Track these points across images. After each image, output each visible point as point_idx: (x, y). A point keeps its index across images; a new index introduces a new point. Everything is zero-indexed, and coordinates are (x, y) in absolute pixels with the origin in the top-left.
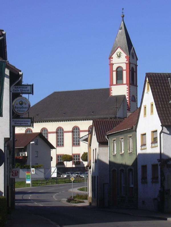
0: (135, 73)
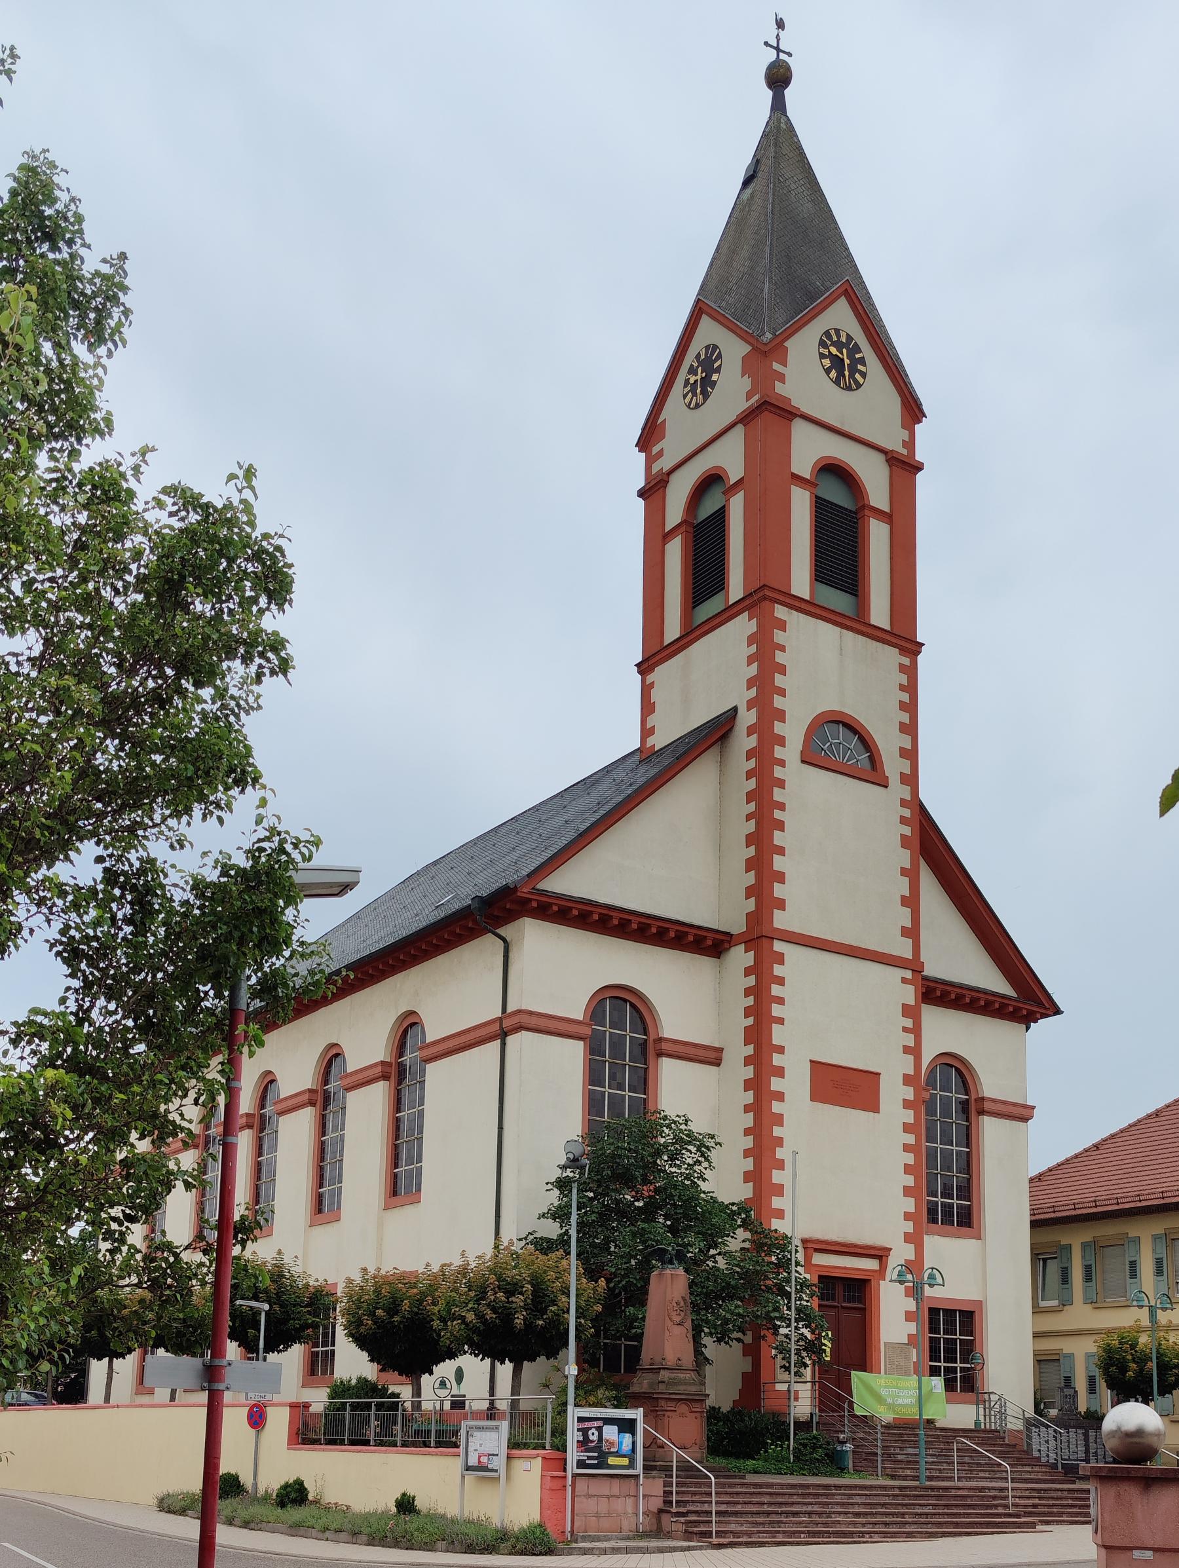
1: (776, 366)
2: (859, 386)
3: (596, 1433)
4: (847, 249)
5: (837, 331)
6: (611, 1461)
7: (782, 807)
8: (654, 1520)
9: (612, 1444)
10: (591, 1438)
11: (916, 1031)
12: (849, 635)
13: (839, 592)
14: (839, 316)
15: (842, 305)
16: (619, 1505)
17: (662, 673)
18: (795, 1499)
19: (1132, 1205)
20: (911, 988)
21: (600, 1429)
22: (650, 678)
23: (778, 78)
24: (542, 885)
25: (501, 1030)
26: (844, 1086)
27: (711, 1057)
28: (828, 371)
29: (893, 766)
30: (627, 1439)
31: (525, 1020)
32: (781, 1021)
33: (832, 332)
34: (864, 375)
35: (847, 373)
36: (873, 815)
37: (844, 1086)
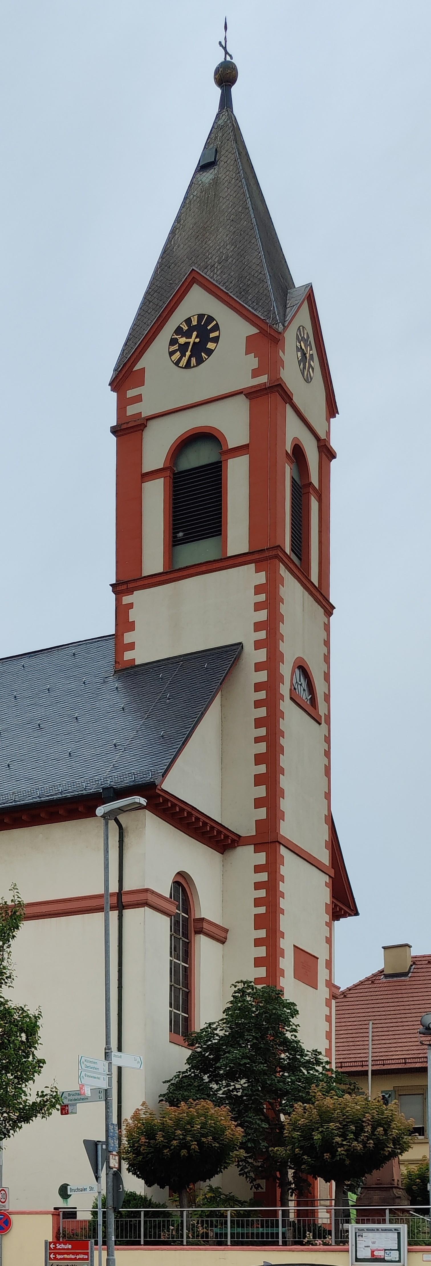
0: (314, 505)
17: (139, 598)
19: (400, 1066)
23: (226, 76)
25: (121, 902)
31: (151, 899)
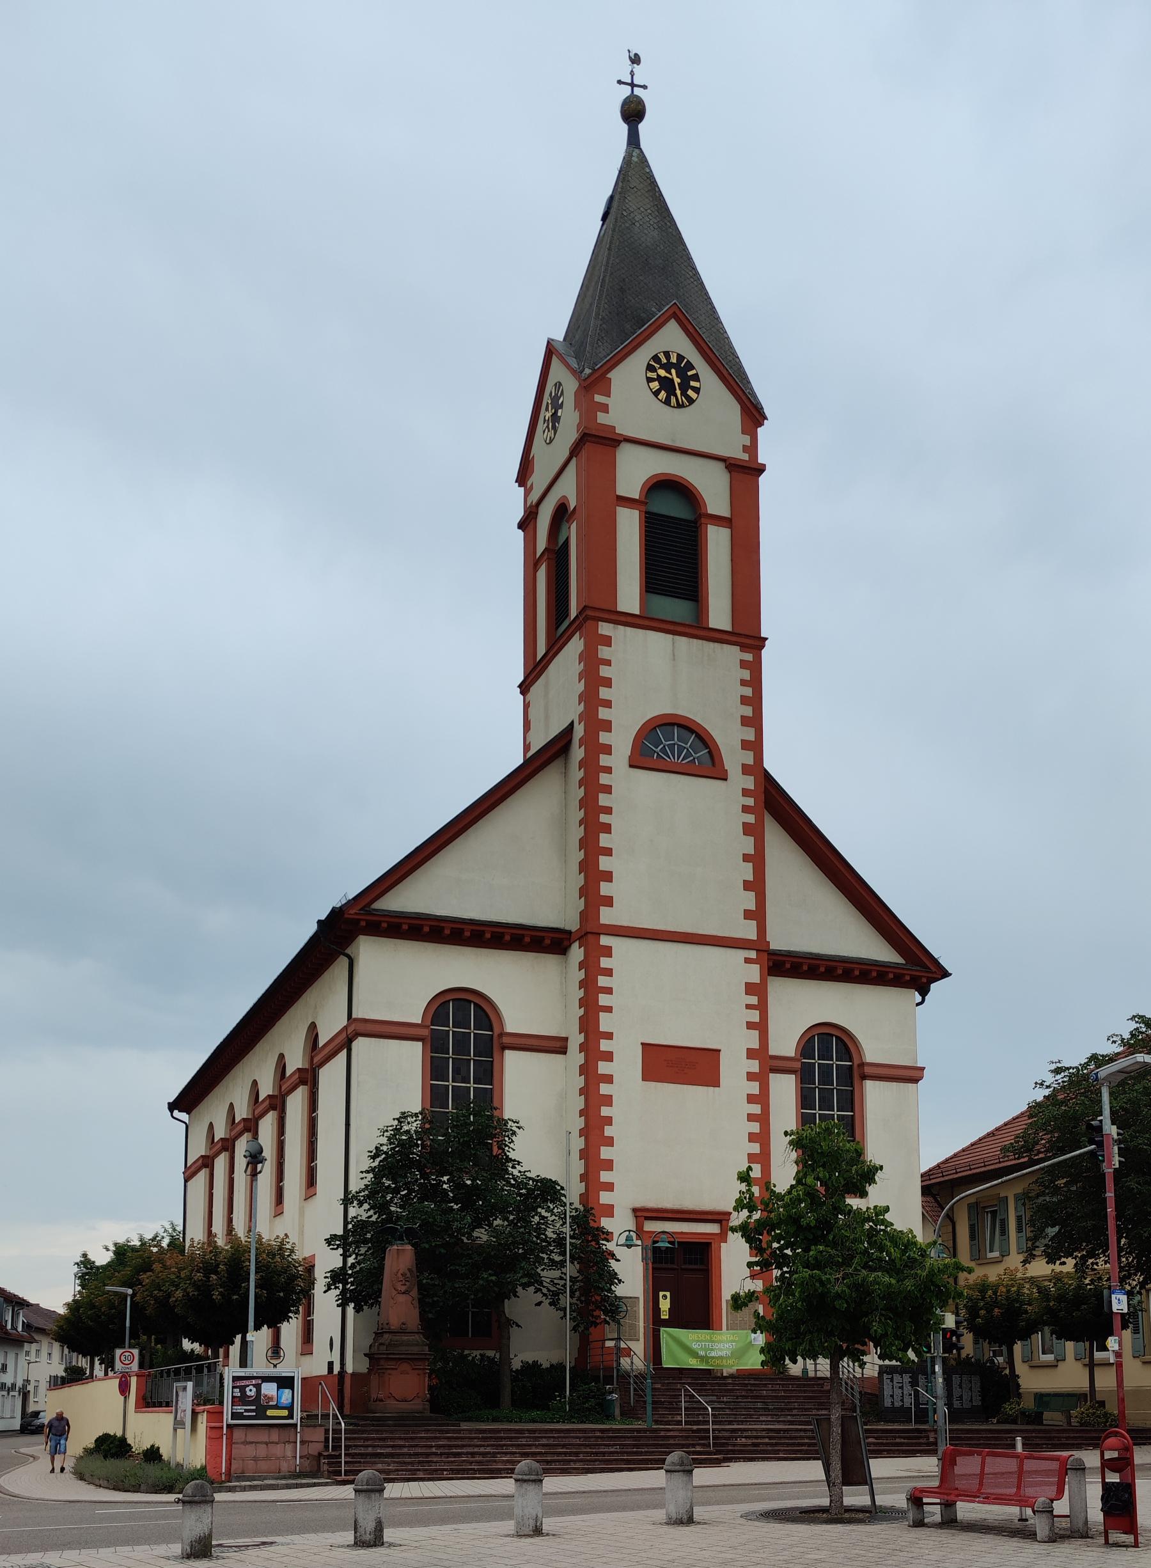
1: (598, 398)
2: (691, 401)
3: (254, 1390)
4: (694, 269)
5: (667, 354)
6: (269, 1413)
7: (608, 810)
8: (315, 1463)
9: (270, 1399)
10: (249, 1393)
11: (762, 1007)
12: (682, 641)
13: (677, 600)
14: (671, 339)
15: (672, 327)
16: (277, 1450)
17: (536, 689)
18: (476, 1442)
20: (756, 968)
21: (258, 1387)
22: (529, 696)
23: (633, 112)
24: (378, 905)
26: (679, 1065)
27: (556, 1046)
28: (656, 394)
29: (733, 758)
30: (286, 1395)
32: (609, 1009)
33: (662, 356)
34: (697, 390)
35: (678, 392)
36: (713, 810)
37: (679, 1065)
